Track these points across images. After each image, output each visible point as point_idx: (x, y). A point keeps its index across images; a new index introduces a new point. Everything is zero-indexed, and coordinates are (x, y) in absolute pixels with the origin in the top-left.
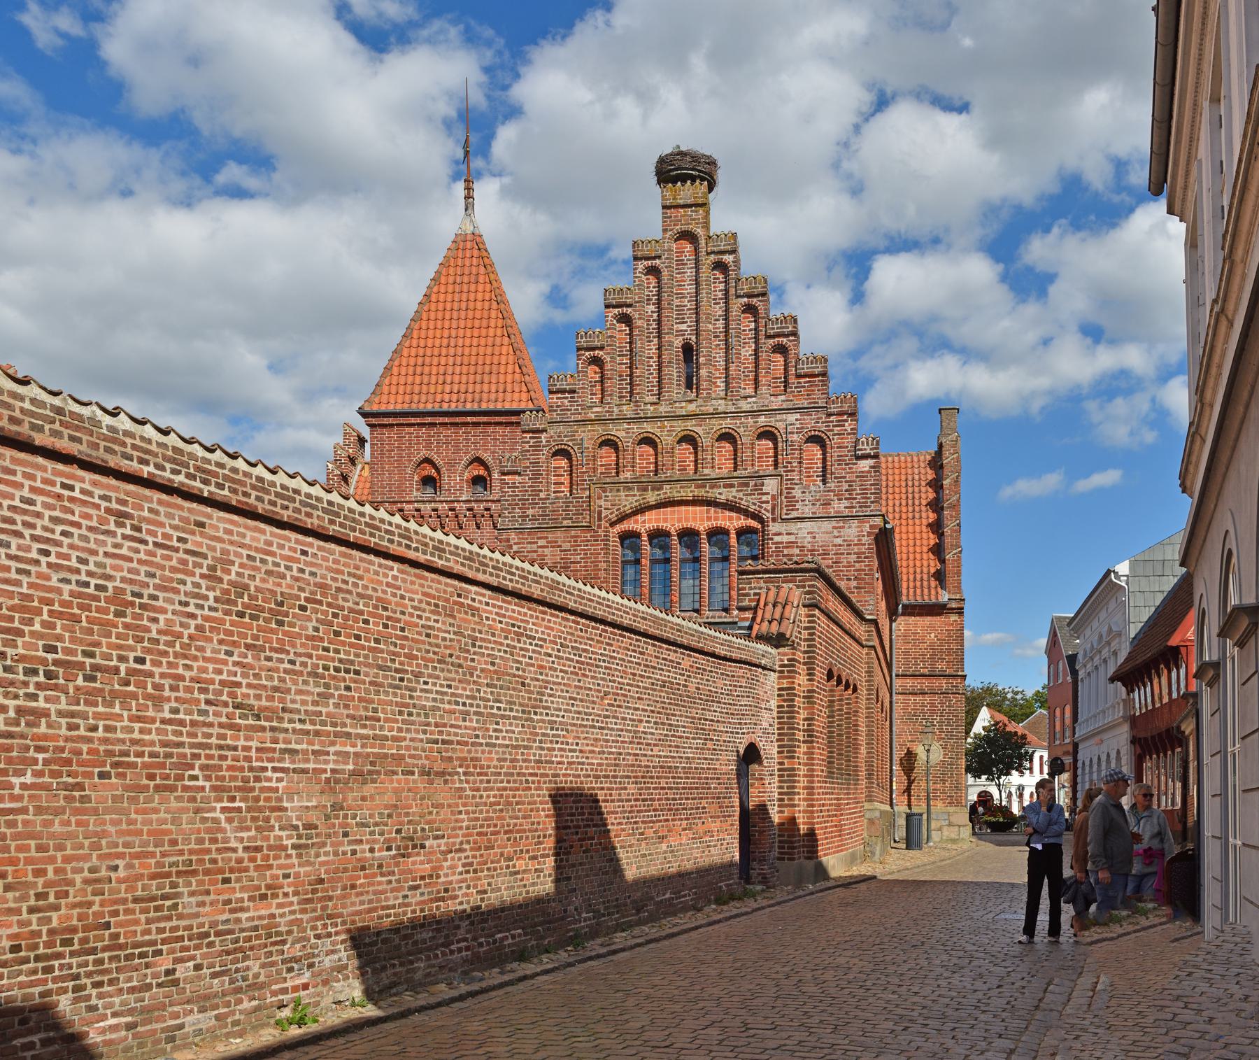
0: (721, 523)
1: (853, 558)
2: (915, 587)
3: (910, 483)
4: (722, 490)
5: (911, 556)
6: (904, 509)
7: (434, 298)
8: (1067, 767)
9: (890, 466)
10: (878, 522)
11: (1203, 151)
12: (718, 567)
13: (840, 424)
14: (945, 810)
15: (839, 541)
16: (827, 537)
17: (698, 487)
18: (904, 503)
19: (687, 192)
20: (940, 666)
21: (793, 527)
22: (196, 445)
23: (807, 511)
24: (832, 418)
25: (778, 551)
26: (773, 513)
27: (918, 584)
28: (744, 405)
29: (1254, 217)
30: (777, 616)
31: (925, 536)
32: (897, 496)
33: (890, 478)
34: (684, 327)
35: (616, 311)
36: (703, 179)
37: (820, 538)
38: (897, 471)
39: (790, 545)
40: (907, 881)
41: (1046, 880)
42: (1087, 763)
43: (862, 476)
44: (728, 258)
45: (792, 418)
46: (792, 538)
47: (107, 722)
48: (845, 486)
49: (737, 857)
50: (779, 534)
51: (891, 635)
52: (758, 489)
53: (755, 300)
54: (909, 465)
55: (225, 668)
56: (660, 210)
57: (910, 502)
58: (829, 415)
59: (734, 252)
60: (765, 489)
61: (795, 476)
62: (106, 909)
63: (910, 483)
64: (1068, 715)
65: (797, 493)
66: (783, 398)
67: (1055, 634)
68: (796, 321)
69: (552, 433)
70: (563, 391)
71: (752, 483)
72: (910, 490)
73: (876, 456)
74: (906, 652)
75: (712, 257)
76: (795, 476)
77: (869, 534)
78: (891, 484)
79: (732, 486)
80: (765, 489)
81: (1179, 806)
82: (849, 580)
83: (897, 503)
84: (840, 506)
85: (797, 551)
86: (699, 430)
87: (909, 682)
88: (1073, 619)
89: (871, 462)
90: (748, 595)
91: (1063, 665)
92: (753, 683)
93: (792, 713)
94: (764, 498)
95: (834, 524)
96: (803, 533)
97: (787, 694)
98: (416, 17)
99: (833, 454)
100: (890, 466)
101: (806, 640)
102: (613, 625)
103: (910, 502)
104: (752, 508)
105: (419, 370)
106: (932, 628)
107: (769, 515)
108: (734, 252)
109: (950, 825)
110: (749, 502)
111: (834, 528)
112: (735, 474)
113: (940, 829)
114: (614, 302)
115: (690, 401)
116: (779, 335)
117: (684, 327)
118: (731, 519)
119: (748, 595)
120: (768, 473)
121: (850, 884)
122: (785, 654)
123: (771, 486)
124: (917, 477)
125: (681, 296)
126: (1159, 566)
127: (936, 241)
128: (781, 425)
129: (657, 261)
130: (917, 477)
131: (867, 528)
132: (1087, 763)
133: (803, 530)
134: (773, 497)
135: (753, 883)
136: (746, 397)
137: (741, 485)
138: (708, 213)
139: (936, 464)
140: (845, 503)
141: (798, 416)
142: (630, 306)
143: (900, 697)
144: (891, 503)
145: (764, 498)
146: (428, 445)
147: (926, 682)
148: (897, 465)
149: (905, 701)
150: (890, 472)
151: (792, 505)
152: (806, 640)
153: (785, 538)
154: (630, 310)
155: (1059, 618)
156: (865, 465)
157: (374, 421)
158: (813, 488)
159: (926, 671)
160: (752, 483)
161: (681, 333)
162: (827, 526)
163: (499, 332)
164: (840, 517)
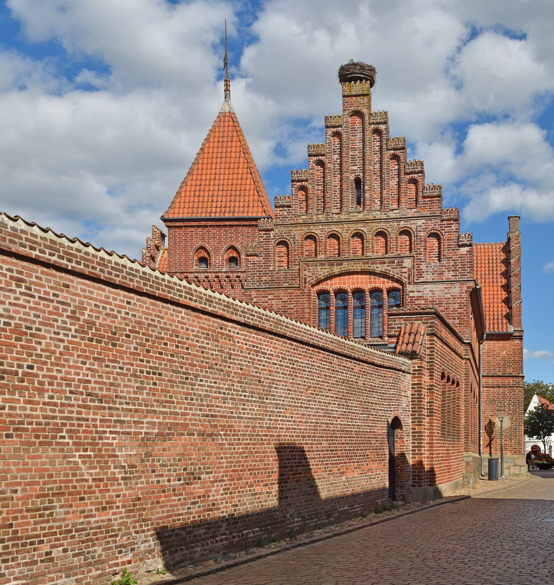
0: (378, 285)
1: (457, 306)
2: (494, 323)
3: (491, 261)
4: (378, 265)
5: (491, 305)
6: (487, 277)
7: (183, 194)
9: (479, 251)
12: (376, 311)
15: (448, 296)
16: (441, 294)
18: (487, 273)
19: (357, 87)
21: (421, 287)
22: (64, 239)
23: (429, 278)
26: (409, 279)
27: (496, 321)
28: (392, 215)
32: (483, 269)
37: (437, 294)
38: (483, 254)
39: (419, 298)
40: (489, 499)
43: (462, 257)
44: (382, 127)
45: (420, 222)
47: (11, 404)
48: (452, 263)
49: (387, 485)
52: (400, 264)
54: (490, 250)
55: (81, 372)
57: (491, 273)
59: (385, 123)
62: (10, 516)
63: (491, 261)
65: (423, 267)
66: (415, 210)
68: (422, 164)
72: (491, 265)
73: (470, 245)
74: (489, 362)
77: (466, 292)
82: (454, 319)
83: (483, 273)
84: (449, 275)
85: (423, 302)
89: (467, 249)
90: (394, 328)
92: (397, 381)
93: (420, 399)
94: (404, 270)
96: (427, 291)
97: (417, 387)
100: (479, 251)
101: (428, 355)
103: (491, 273)
104: (396, 276)
107: (407, 280)
108: (385, 123)
110: (394, 272)
111: (445, 288)
112: (386, 256)
114: (314, 153)
116: (412, 173)
118: (384, 282)
120: (406, 255)
121: (455, 501)
123: (407, 263)
124: (495, 258)
125: (354, 149)
127: (506, 117)
128: (413, 227)
129: (340, 129)
130: (495, 258)
134: (409, 269)
135: (397, 500)
136: (393, 210)
137: (389, 262)
139: (507, 249)
140: (452, 273)
142: (323, 155)
143: (485, 389)
144: (479, 273)
145: (404, 270)
148: (483, 250)
150: (479, 254)
151: (420, 274)
152: (428, 355)
153: (416, 294)
154: (323, 158)
156: (464, 250)
158: (432, 264)
161: (354, 171)
162: (441, 287)
163: (245, 171)
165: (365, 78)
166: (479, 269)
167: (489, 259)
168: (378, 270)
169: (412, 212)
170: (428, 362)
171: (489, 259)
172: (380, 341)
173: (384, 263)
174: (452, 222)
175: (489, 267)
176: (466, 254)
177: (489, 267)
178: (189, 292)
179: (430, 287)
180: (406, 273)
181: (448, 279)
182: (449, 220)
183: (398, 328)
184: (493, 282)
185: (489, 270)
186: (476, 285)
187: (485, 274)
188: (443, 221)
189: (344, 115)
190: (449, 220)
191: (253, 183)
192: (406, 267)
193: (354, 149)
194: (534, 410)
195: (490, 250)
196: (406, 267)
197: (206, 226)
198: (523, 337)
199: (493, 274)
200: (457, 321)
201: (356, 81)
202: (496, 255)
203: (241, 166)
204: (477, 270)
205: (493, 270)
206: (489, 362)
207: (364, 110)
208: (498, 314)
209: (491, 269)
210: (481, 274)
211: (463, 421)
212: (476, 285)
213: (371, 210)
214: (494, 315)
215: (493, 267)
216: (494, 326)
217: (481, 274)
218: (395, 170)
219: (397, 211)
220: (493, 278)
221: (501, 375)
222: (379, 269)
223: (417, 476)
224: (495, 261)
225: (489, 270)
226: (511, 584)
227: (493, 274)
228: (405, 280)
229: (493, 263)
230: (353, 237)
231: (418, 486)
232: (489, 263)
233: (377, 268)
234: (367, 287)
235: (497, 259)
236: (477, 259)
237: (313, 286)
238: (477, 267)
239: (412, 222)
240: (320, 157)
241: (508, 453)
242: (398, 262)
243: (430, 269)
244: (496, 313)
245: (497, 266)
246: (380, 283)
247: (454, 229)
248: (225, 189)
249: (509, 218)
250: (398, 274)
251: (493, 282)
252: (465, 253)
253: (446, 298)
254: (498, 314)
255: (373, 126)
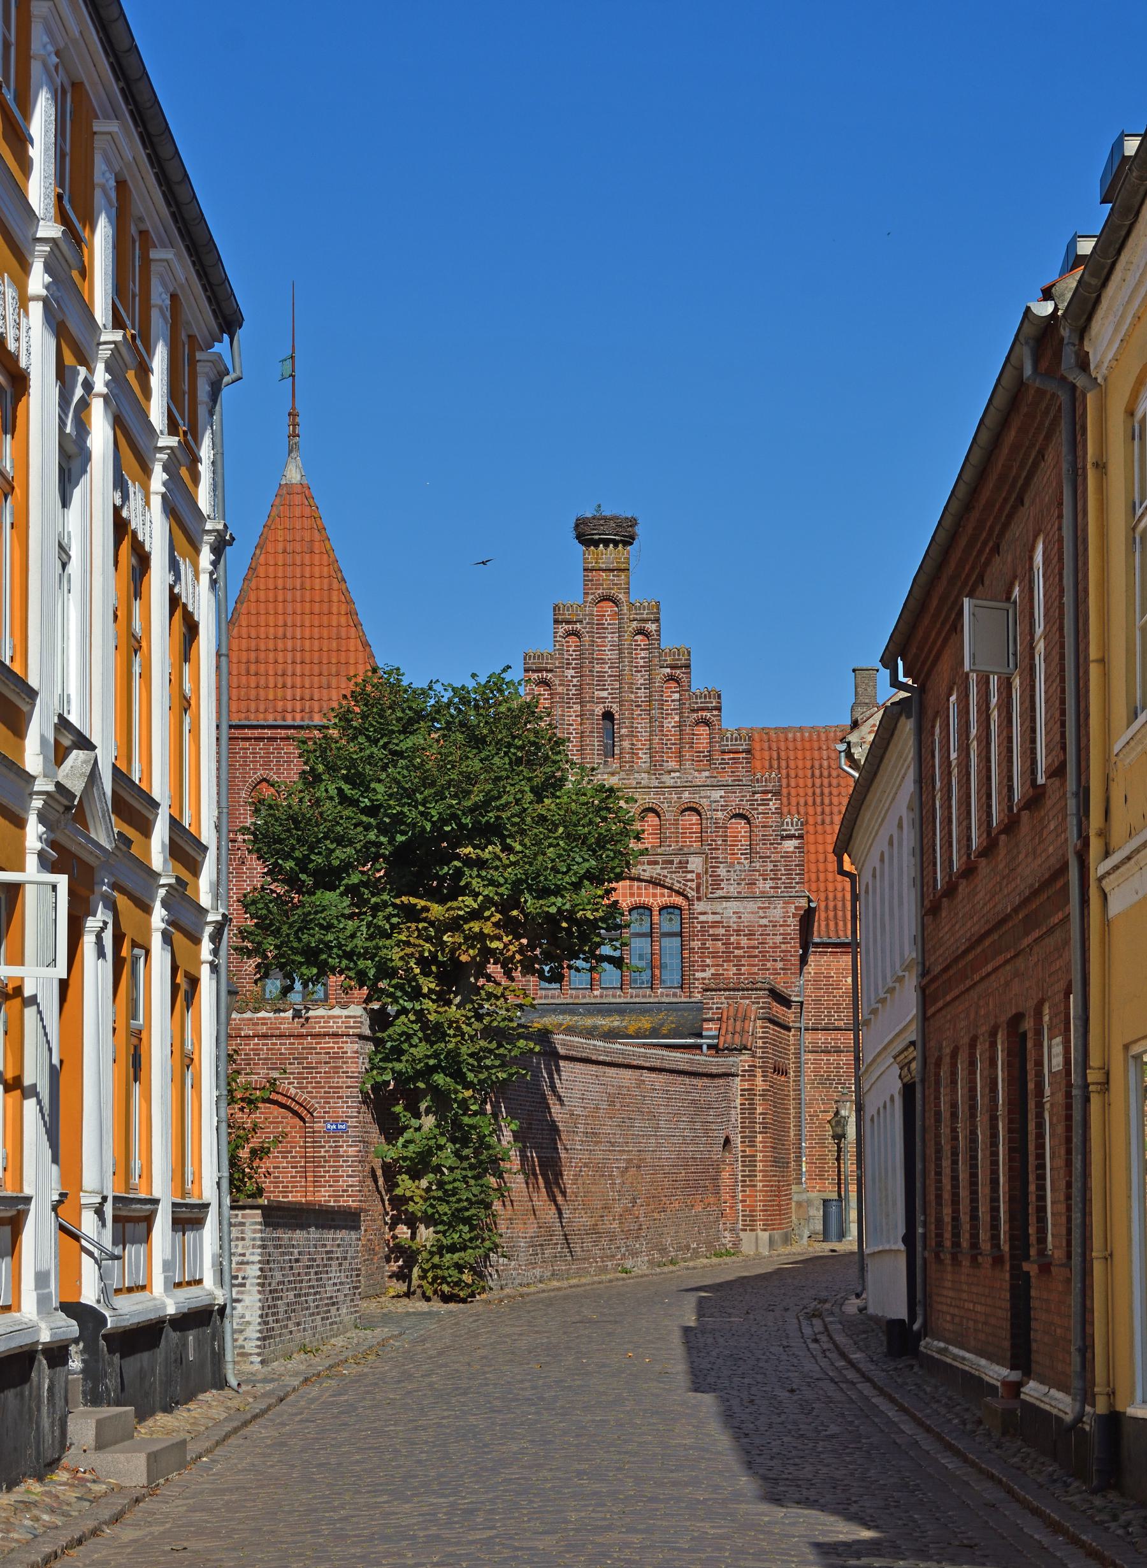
0: (643, 899)
1: (779, 939)
2: (827, 919)
3: (817, 773)
4: (646, 867)
5: (822, 876)
6: (811, 810)
7: (261, 571)
9: (791, 746)
11: (815, 928)
15: (764, 922)
16: (753, 918)
18: (810, 802)
19: (608, 555)
21: (719, 907)
22: (133, 512)
23: (733, 890)
24: (757, 796)
25: (703, 931)
26: (698, 891)
27: (831, 914)
28: (668, 780)
30: (738, 1029)
31: (830, 876)
32: (801, 792)
33: (792, 764)
34: (604, 694)
37: (746, 918)
38: (800, 754)
39: (715, 925)
41: (866, 1534)
43: (787, 856)
44: (651, 627)
45: (717, 794)
46: (717, 918)
48: (770, 866)
50: (705, 913)
51: (1061, 569)
52: (683, 865)
54: (816, 745)
56: (582, 573)
57: (818, 800)
59: (657, 620)
60: (690, 867)
61: (719, 854)
63: (817, 773)
65: (722, 871)
66: (707, 774)
68: (719, 697)
72: (818, 782)
73: (801, 837)
74: (817, 1001)
75: (635, 624)
76: (719, 854)
77: (794, 916)
78: (792, 773)
81: (259, 1212)
82: (775, 961)
83: (802, 801)
84: (765, 886)
85: (722, 931)
89: (795, 842)
90: (711, 1008)
94: (689, 876)
96: (729, 913)
97: (749, 1094)
98: (34, 1100)
99: (759, 832)
100: (791, 746)
101: (761, 1048)
102: (672, 1071)
103: (818, 800)
104: (677, 886)
105: (253, 668)
106: (695, 1398)
107: (694, 894)
108: (657, 620)
111: (759, 908)
112: (659, 851)
114: (534, 667)
115: (613, 774)
116: (702, 709)
117: (604, 694)
118: (655, 895)
119: (711, 1008)
120: (692, 850)
122: (746, 1061)
123: (696, 864)
124: (825, 763)
125: (602, 662)
127: (986, 1504)
128: (704, 802)
129: (578, 626)
130: (825, 763)
133: (730, 908)
134: (698, 876)
136: (669, 772)
137: (665, 862)
138: (628, 577)
139: (60, 546)
140: (769, 883)
141: (722, 793)
142: (551, 671)
143: (810, 1056)
144: (794, 801)
145: (689, 876)
146: (267, 764)
148: (799, 744)
150: (792, 755)
151: (717, 883)
152: (761, 1048)
153: (710, 918)
154: (550, 675)
156: (790, 845)
158: (738, 867)
161: (602, 700)
162: (752, 906)
163: (343, 620)
164: (764, 895)
165: (622, 541)
166: (793, 792)
167: (812, 767)
168: (646, 875)
169: (702, 777)
170: (761, 1058)
171: (812, 767)
172: (620, 996)
173: (656, 863)
174: (770, 796)
175: (813, 786)
176: (794, 852)
177: (813, 786)
178: (941, 790)
179: (733, 906)
180: (692, 880)
181: (763, 892)
182: (765, 792)
183: (718, 1008)
184: (823, 823)
185: (814, 794)
186: (810, 901)
187: (806, 804)
188: (754, 793)
189: (585, 602)
190: (765, 792)
191: (361, 648)
192: (692, 872)
193: (602, 662)
194: (1021, 1030)
195: (816, 745)
196: (692, 872)
197: (272, 739)
198: (638, 529)
199: (822, 803)
200: (780, 965)
201: (606, 546)
202: (829, 758)
203: (335, 610)
204: (789, 794)
205: (822, 794)
206: (817, 1001)
207: (621, 596)
208: (835, 898)
209: (818, 791)
210: (798, 804)
211: (984, 535)
212: (810, 901)
213: (631, 771)
214: (827, 899)
215: (822, 785)
216: (827, 925)
217: (798, 804)
218: (673, 701)
219: (677, 774)
220: (823, 813)
221: (844, 1027)
222: (647, 874)
223: (749, 1206)
224: (826, 773)
225: (814, 794)
226: (14, 1085)
227: (822, 803)
228: (692, 894)
229: (821, 776)
230: (390, 1277)
231: (751, 1230)
232: (813, 776)
233: (644, 871)
234: (1068, 835)
235: (829, 767)
236: (787, 767)
237: (694, 711)
238: (788, 785)
239: (703, 794)
240: (545, 674)
241: (422, 1227)
242: (680, 862)
243: (733, 876)
244: (831, 896)
245: (830, 785)
246: (647, 896)
247: (773, 808)
248: (262, 598)
249: (854, 671)
250: (679, 882)
251: (823, 823)
252: (791, 849)
253: (761, 926)
254: (835, 898)
255: (635, 624)
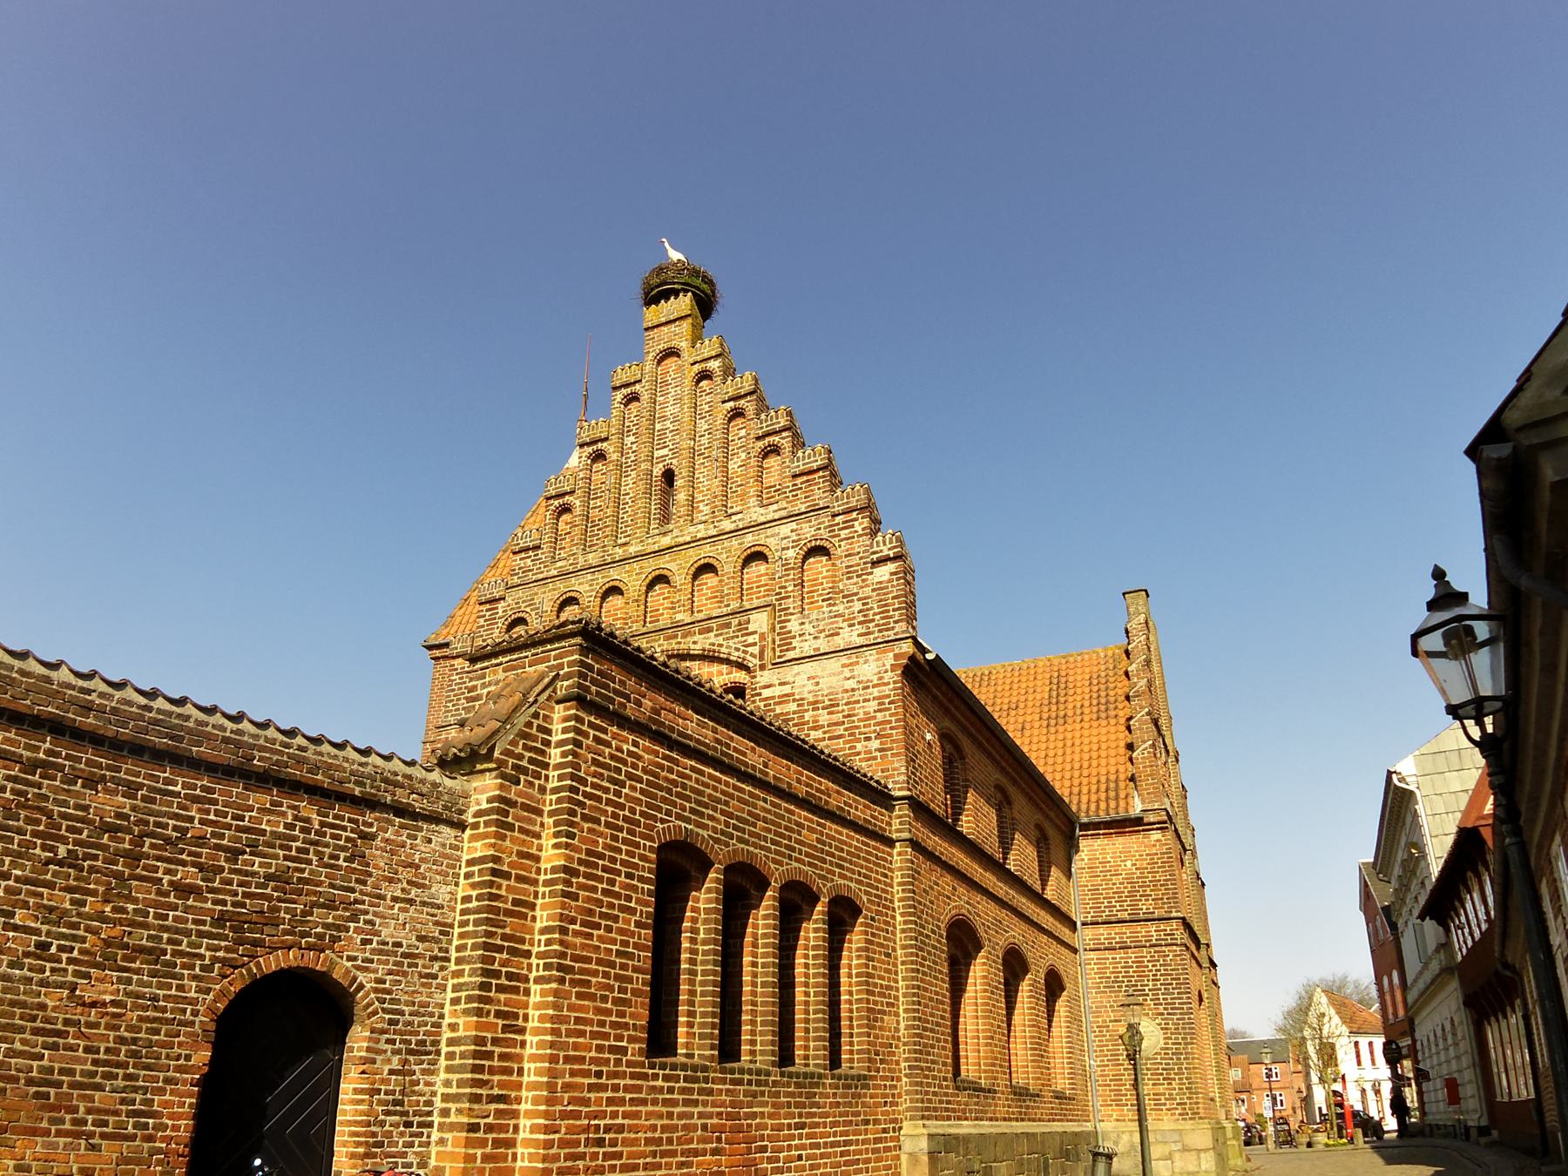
1: (873, 705)
4: (697, 637)
8: (1404, 1051)
10: (907, 648)
13: (848, 525)
14: (1174, 1126)
15: (851, 684)
17: (668, 638)
20: (1144, 907)
21: (789, 673)
23: (807, 648)
29: (1556, 797)
35: (590, 449)
36: (686, 291)
37: (825, 684)
42: (1425, 1043)
43: (880, 588)
45: (785, 530)
46: (787, 689)
48: (858, 606)
50: (769, 686)
52: (743, 629)
53: (742, 402)
58: (834, 516)
60: (751, 628)
64: (1396, 980)
67: (1366, 885)
69: (509, 600)
70: (526, 550)
71: (735, 622)
79: (710, 630)
80: (751, 628)
82: (868, 739)
85: (793, 707)
86: (673, 566)
87: (1103, 931)
88: (1375, 863)
91: (1381, 920)
94: (750, 639)
95: (845, 660)
106: (1127, 854)
107: (757, 662)
109: (1186, 1149)
111: (844, 666)
113: (1169, 1157)
126: (1454, 758)
128: (772, 542)
131: (889, 660)
132: (1425, 1043)
140: (861, 629)
141: (794, 526)
145: (750, 639)
147: (1125, 929)
149: (1100, 961)
153: (777, 691)
155: (1363, 864)
157: (437, 653)
159: (1125, 916)
160: (735, 622)
162: (833, 664)
